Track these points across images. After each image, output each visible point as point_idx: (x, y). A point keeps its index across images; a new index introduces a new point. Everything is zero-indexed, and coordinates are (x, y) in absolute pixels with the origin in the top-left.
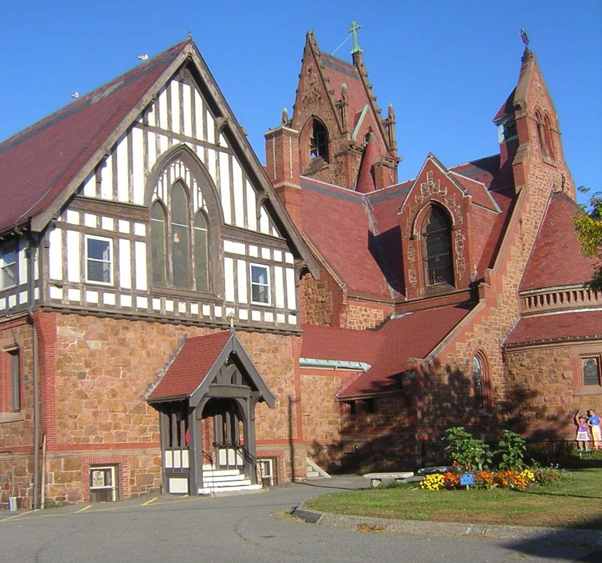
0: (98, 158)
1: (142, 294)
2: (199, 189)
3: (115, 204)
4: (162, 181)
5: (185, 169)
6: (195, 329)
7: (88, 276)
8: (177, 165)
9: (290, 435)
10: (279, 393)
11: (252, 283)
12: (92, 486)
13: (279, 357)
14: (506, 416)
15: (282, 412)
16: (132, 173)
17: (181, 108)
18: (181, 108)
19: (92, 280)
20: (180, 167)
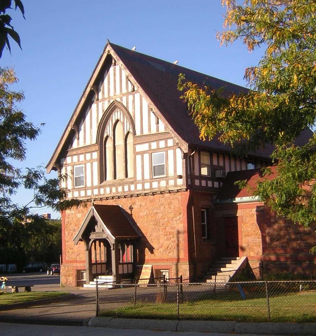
0: (69, 131)
1: (96, 188)
2: (128, 120)
3: (158, 134)
4: (109, 125)
5: (120, 112)
6: (122, 199)
7: (163, 175)
8: (116, 113)
9: (178, 256)
10: (172, 230)
11: (75, 177)
12: (60, 286)
13: (172, 207)
14: (26, 252)
15: (173, 242)
16: (92, 128)
17: (115, 80)
18: (115, 80)
19: (160, 175)
20: (117, 113)
